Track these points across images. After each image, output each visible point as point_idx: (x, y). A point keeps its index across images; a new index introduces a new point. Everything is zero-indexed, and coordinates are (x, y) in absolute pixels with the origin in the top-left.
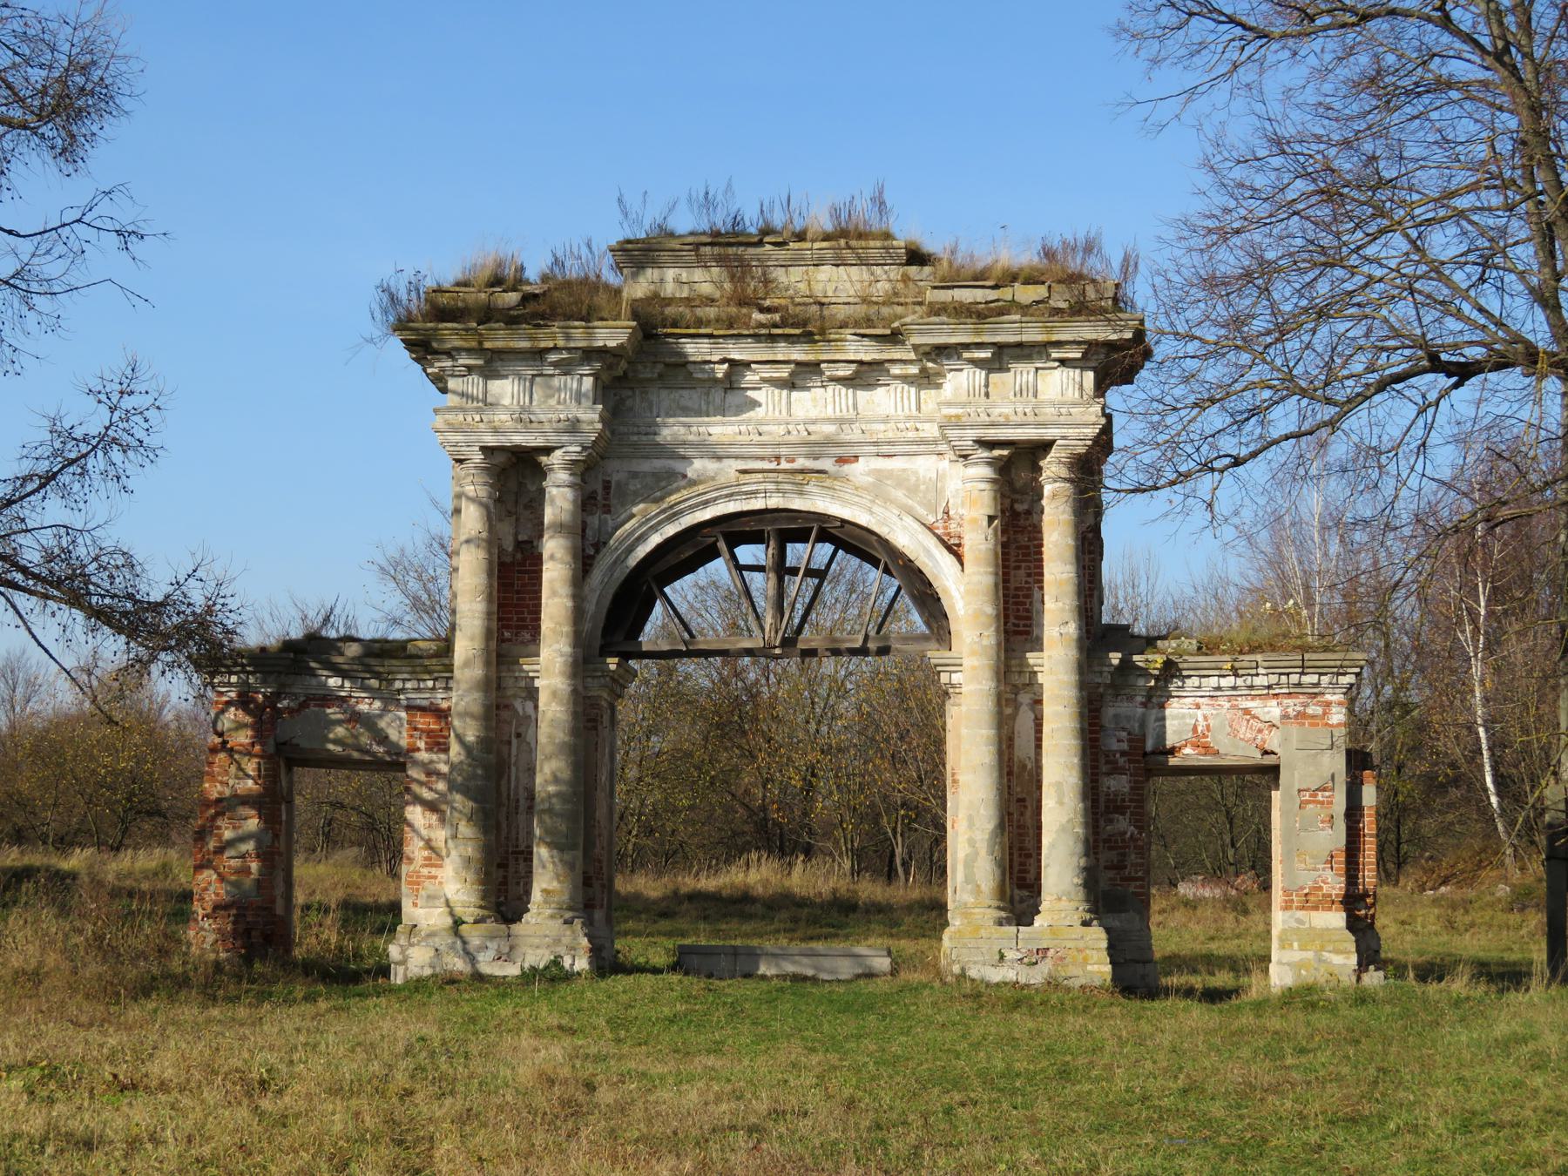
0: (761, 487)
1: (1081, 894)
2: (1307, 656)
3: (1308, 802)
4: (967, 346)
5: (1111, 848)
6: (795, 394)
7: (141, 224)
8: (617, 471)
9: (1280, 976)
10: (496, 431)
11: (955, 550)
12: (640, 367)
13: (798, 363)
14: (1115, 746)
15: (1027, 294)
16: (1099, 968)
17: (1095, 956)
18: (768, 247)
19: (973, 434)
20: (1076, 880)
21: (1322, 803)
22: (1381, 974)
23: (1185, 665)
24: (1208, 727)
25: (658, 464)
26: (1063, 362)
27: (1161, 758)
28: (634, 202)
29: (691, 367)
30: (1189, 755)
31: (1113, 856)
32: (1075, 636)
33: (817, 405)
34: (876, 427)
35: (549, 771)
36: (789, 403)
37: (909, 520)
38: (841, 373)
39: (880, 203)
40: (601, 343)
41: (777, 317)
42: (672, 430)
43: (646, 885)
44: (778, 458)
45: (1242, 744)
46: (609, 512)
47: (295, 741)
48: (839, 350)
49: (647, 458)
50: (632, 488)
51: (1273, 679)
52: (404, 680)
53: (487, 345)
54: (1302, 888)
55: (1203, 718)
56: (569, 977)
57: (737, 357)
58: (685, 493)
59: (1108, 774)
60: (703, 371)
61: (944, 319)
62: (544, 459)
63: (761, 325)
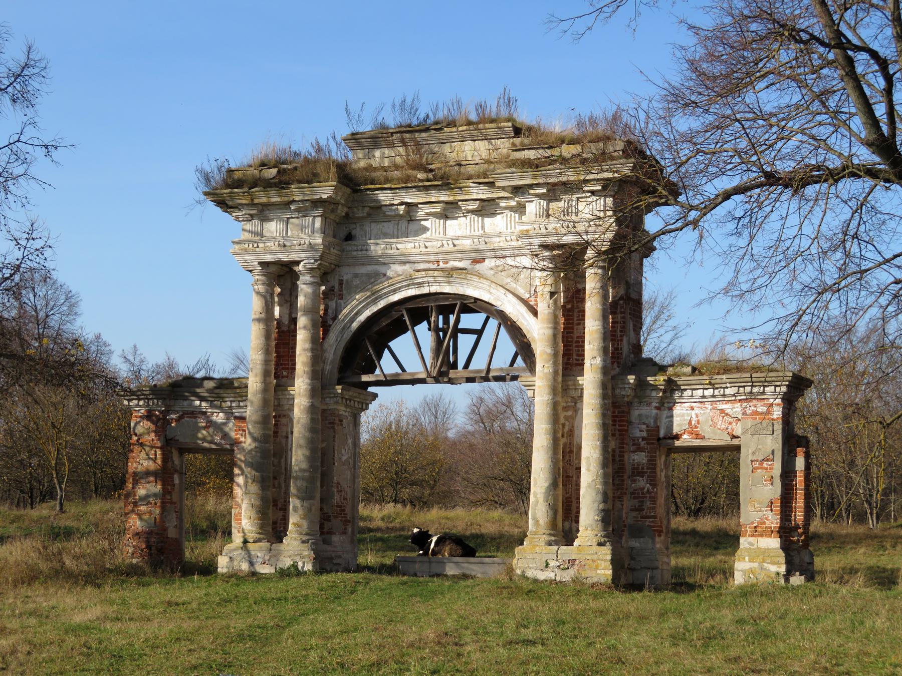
0: (425, 280)
1: (600, 526)
2: (754, 375)
3: (758, 468)
4: (531, 186)
5: (634, 498)
6: (448, 222)
7: (60, 140)
8: (346, 274)
10: (271, 253)
11: (535, 313)
12: (355, 210)
13: (447, 203)
14: (638, 434)
15: (568, 151)
16: (605, 572)
17: (603, 564)
18: (433, 132)
19: (537, 241)
20: (596, 518)
21: (766, 469)
22: (803, 577)
23: (681, 383)
24: (698, 421)
25: (370, 269)
26: (593, 193)
27: (669, 441)
28: (354, 109)
29: (384, 208)
30: (686, 440)
31: (636, 503)
32: (600, 366)
33: (461, 229)
34: (494, 240)
35: (298, 457)
36: (445, 228)
37: (510, 296)
38: (471, 207)
39: (509, 102)
40: (318, 197)
41: (430, 176)
42: (377, 248)
44: (438, 261)
45: (719, 432)
46: (342, 298)
47: (177, 438)
48: (467, 193)
49: (363, 265)
50: (354, 283)
51: (735, 390)
52: (231, 401)
53: (256, 201)
54: (753, 523)
55: (697, 417)
56: (299, 574)
57: (409, 201)
58: (386, 284)
59: (634, 452)
60: (391, 210)
61: (514, 170)
62: (296, 269)
63: (421, 181)
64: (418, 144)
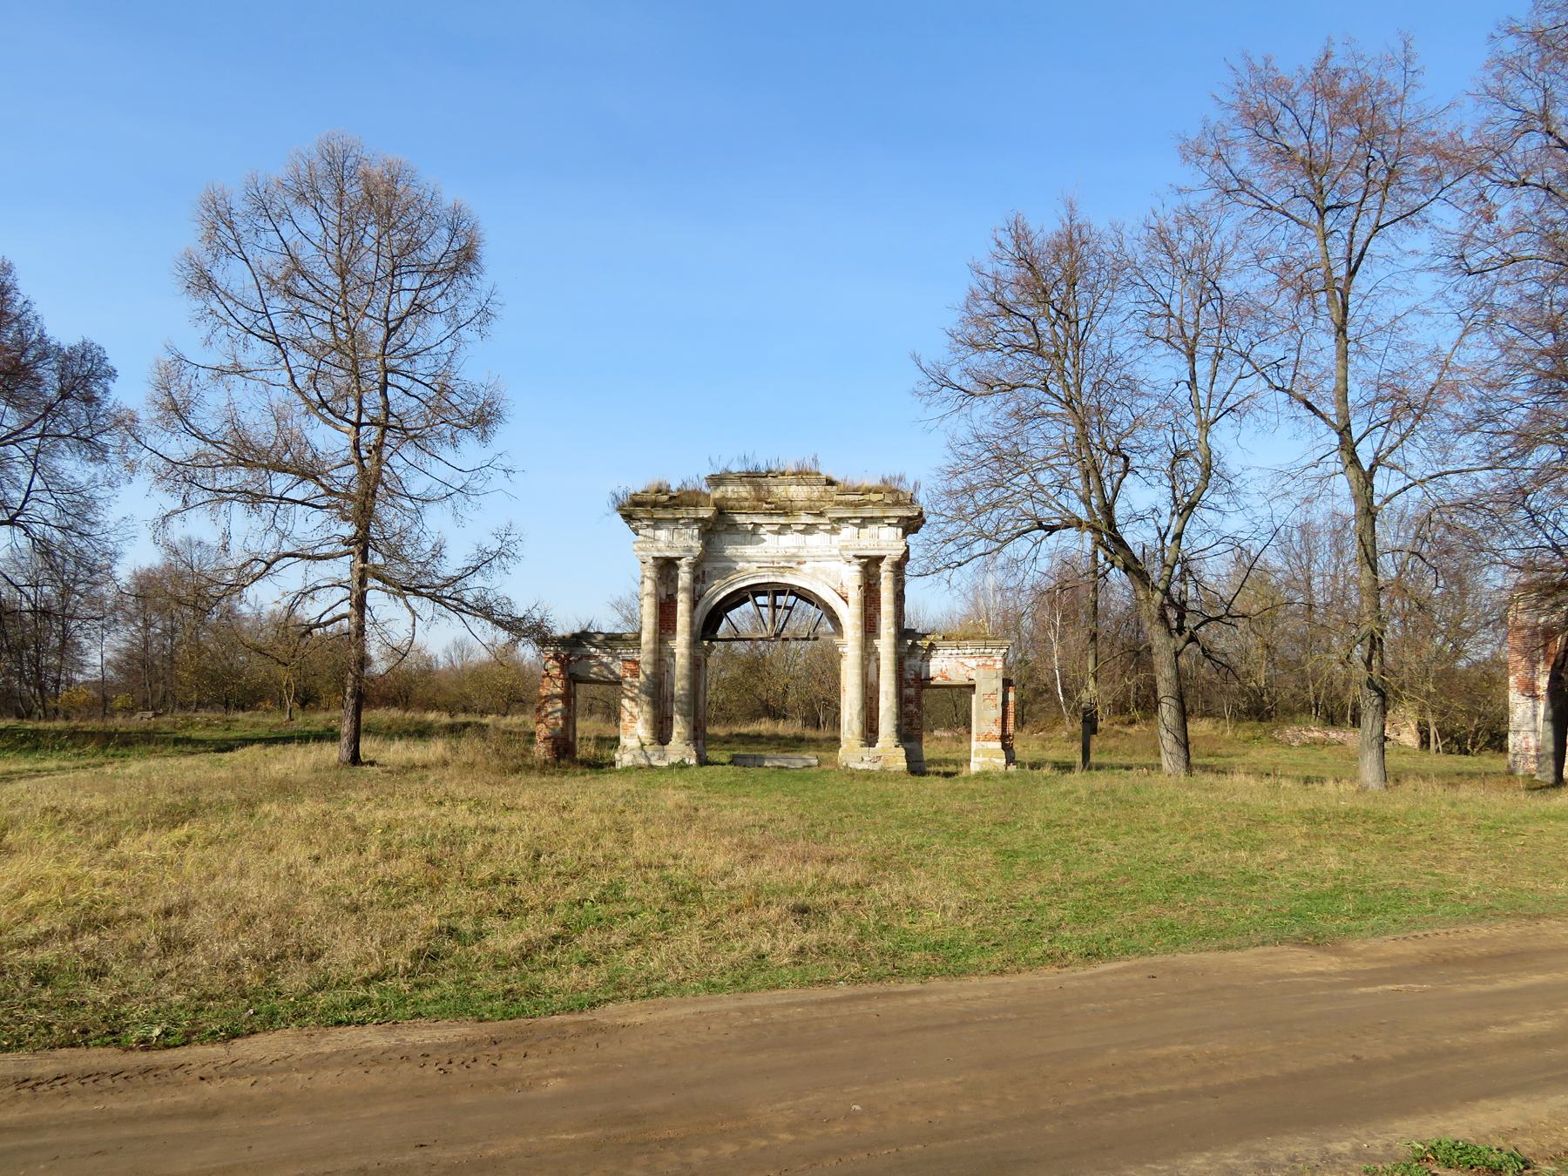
8: (708, 567)
9: (975, 767)
11: (845, 599)
15: (875, 497)
16: (901, 764)
28: (715, 459)
30: (939, 681)
33: (790, 541)
35: (680, 686)
39: (815, 460)
42: (730, 551)
43: (719, 730)
55: (945, 666)
56: (688, 766)
64: (760, 485)
